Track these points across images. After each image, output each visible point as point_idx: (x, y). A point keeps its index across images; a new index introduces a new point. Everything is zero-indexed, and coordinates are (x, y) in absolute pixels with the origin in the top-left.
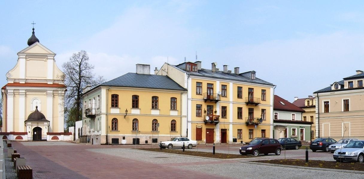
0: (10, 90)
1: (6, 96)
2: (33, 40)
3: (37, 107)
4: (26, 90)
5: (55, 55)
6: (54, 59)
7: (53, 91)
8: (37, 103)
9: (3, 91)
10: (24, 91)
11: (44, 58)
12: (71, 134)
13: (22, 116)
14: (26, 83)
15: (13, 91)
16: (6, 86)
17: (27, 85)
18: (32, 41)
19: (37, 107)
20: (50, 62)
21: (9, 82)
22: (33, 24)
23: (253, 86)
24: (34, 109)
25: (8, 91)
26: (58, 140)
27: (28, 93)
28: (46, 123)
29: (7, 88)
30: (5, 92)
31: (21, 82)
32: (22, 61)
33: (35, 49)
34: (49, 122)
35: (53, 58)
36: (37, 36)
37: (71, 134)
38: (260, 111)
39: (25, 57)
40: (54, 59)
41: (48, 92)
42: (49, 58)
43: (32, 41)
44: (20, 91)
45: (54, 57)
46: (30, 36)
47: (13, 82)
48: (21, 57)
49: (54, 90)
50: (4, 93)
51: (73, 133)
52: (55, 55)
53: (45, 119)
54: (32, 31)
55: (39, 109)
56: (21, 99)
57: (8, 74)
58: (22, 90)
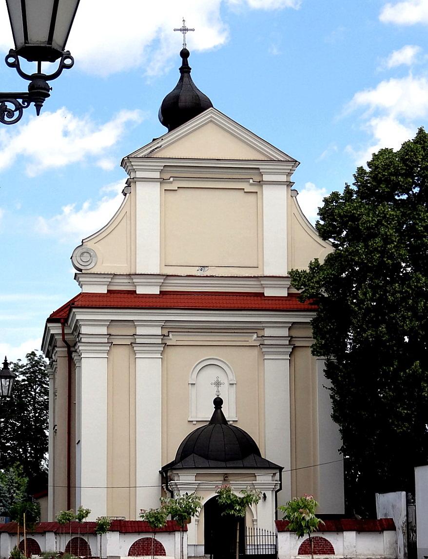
0: (92, 324)
1: (70, 353)
2: (185, 100)
3: (218, 403)
4: (165, 325)
5: (295, 163)
6: (290, 184)
7: (108, 327)
8: (218, 384)
9: (56, 329)
10: (158, 331)
11: (245, 180)
12: (389, 525)
13: (154, 450)
14: (162, 293)
15: (104, 330)
16: (70, 307)
17: (166, 300)
18: (182, 107)
19: (218, 403)
20: (274, 198)
21: (88, 289)
22: (184, 30)
23: (97, 238)
24: (207, 413)
25: (84, 330)
26: (332, 556)
27: (173, 339)
28: (264, 479)
29: (80, 315)
30: (63, 334)
31: (268, 293)
32: (149, 195)
33: (198, 140)
34: (281, 469)
35: (284, 178)
36: (201, 81)
37: (389, 525)
38: (297, 549)
39: (157, 175)
40: (290, 184)
41: (268, 332)
42: (266, 178)
43: (182, 107)
44: (140, 331)
45: (289, 174)
46: (170, 85)
47: (103, 290)
48: (139, 174)
49: (294, 323)
50: (59, 338)
51: (400, 521)
52: (295, 163)
53: (259, 455)
54: (180, 62)
55: (229, 412)
56: (148, 369)
57: (80, 251)
58: (148, 324)
